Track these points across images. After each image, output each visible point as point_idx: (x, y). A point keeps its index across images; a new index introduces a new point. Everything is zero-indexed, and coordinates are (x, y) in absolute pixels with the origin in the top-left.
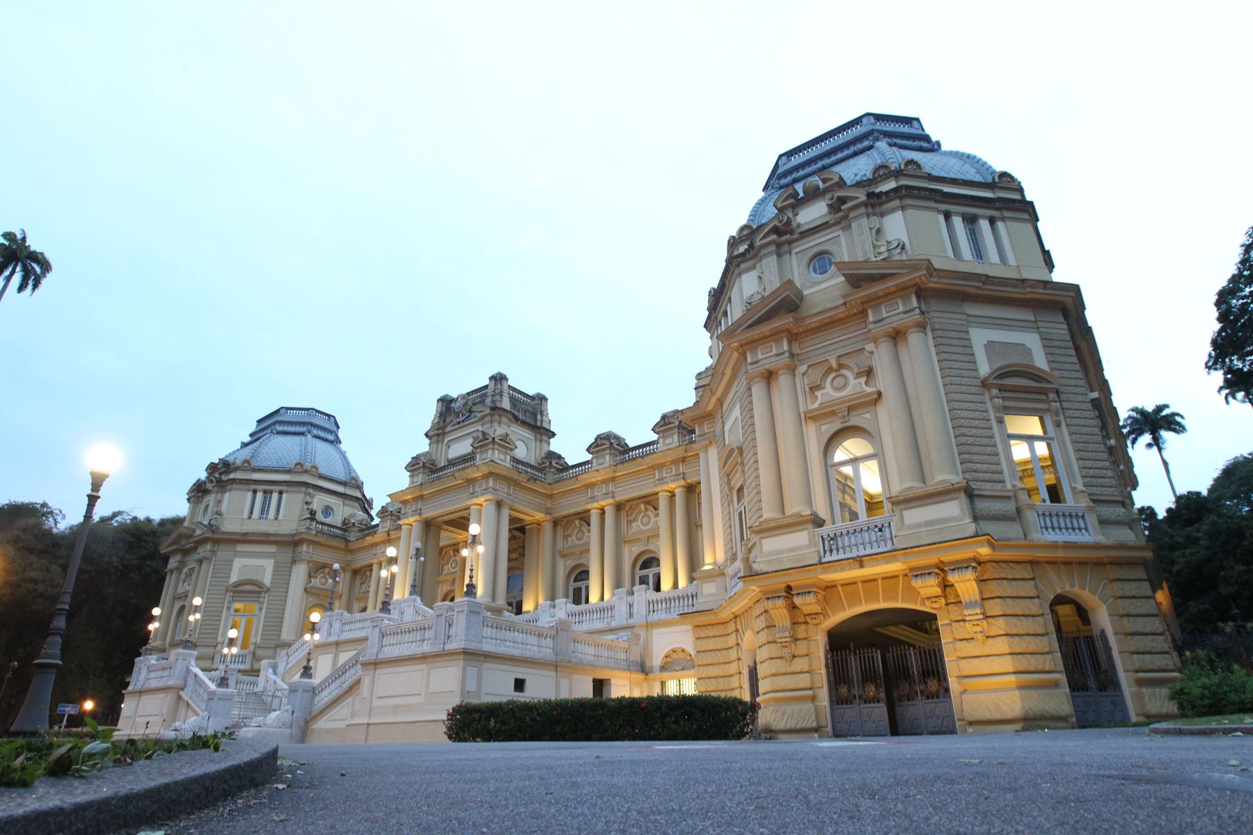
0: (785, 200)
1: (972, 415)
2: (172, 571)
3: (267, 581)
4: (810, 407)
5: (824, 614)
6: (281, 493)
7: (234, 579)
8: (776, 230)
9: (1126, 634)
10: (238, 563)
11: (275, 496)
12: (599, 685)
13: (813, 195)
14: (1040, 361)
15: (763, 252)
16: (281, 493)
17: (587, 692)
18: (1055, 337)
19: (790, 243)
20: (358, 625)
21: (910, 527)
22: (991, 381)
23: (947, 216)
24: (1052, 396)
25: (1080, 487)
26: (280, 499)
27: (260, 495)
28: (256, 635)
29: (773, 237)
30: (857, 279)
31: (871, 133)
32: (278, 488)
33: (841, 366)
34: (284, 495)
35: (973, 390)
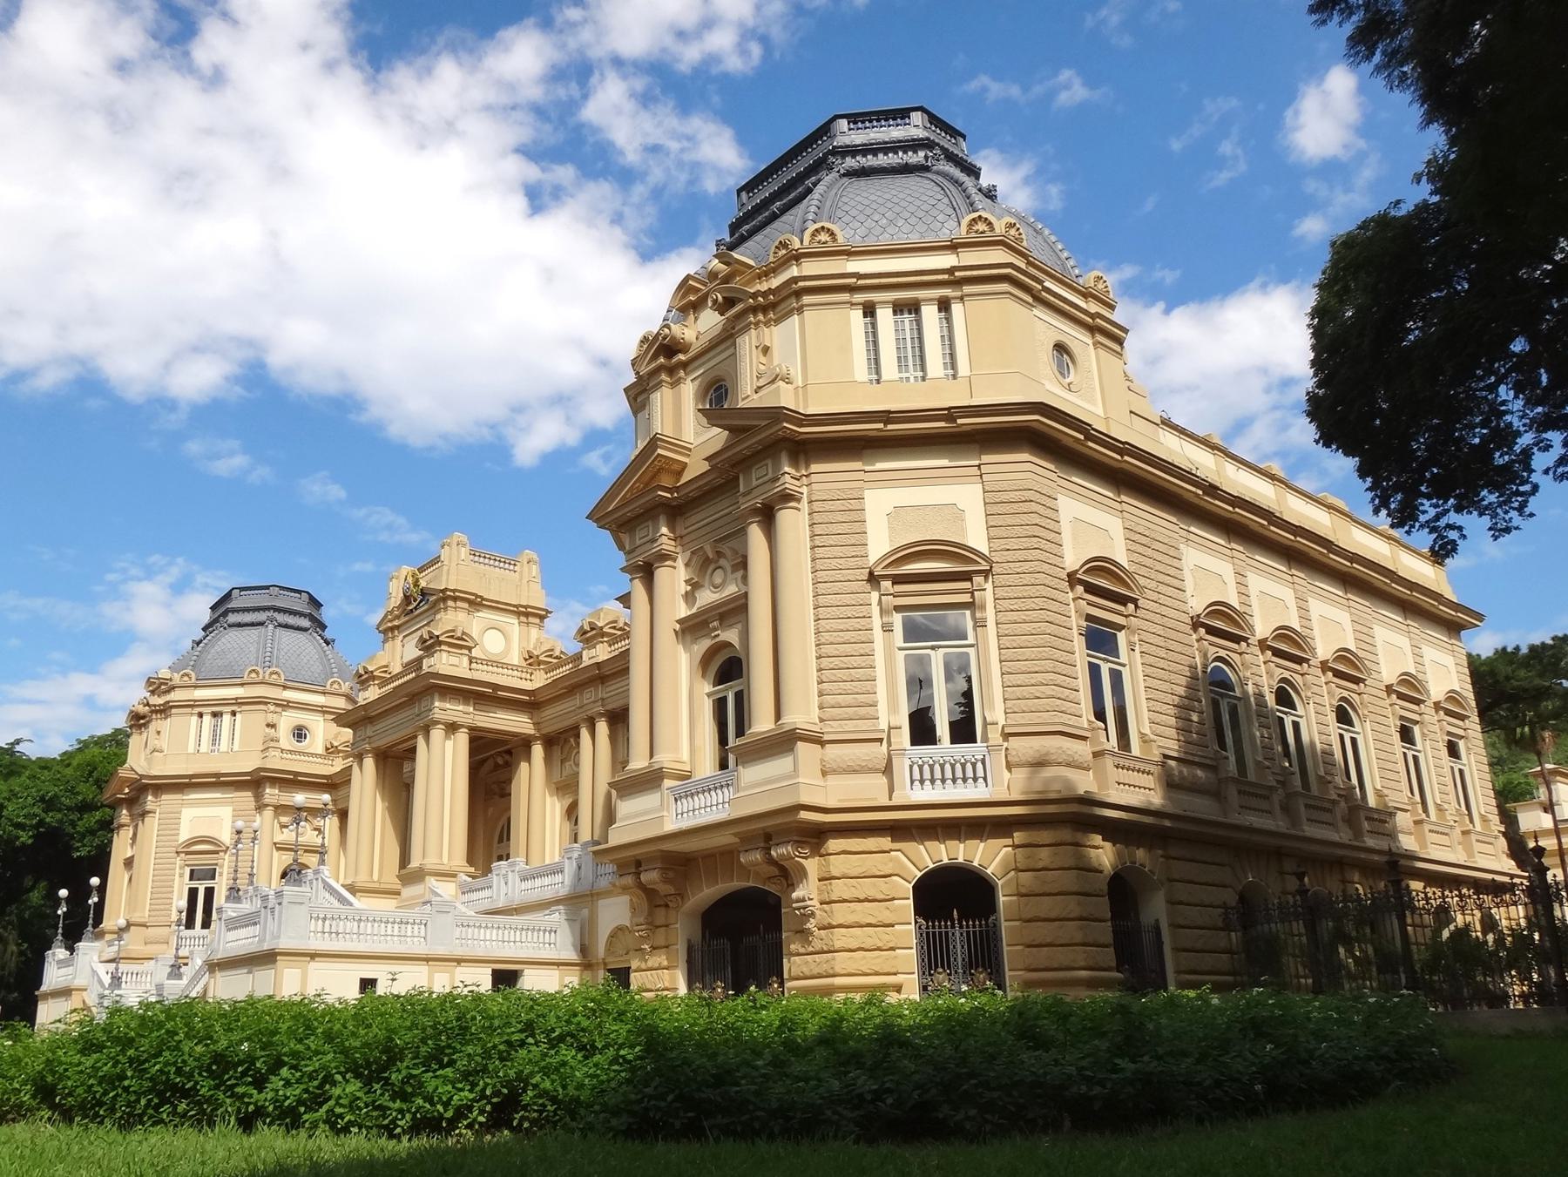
1: (842, 624)
3: (976, 537)
5: (681, 895)
7: (184, 836)
10: (188, 814)
12: (505, 978)
16: (234, 714)
17: (352, 993)
18: (1005, 486)
23: (869, 311)
31: (926, 144)
33: (719, 554)
34: (957, 309)
35: (855, 586)
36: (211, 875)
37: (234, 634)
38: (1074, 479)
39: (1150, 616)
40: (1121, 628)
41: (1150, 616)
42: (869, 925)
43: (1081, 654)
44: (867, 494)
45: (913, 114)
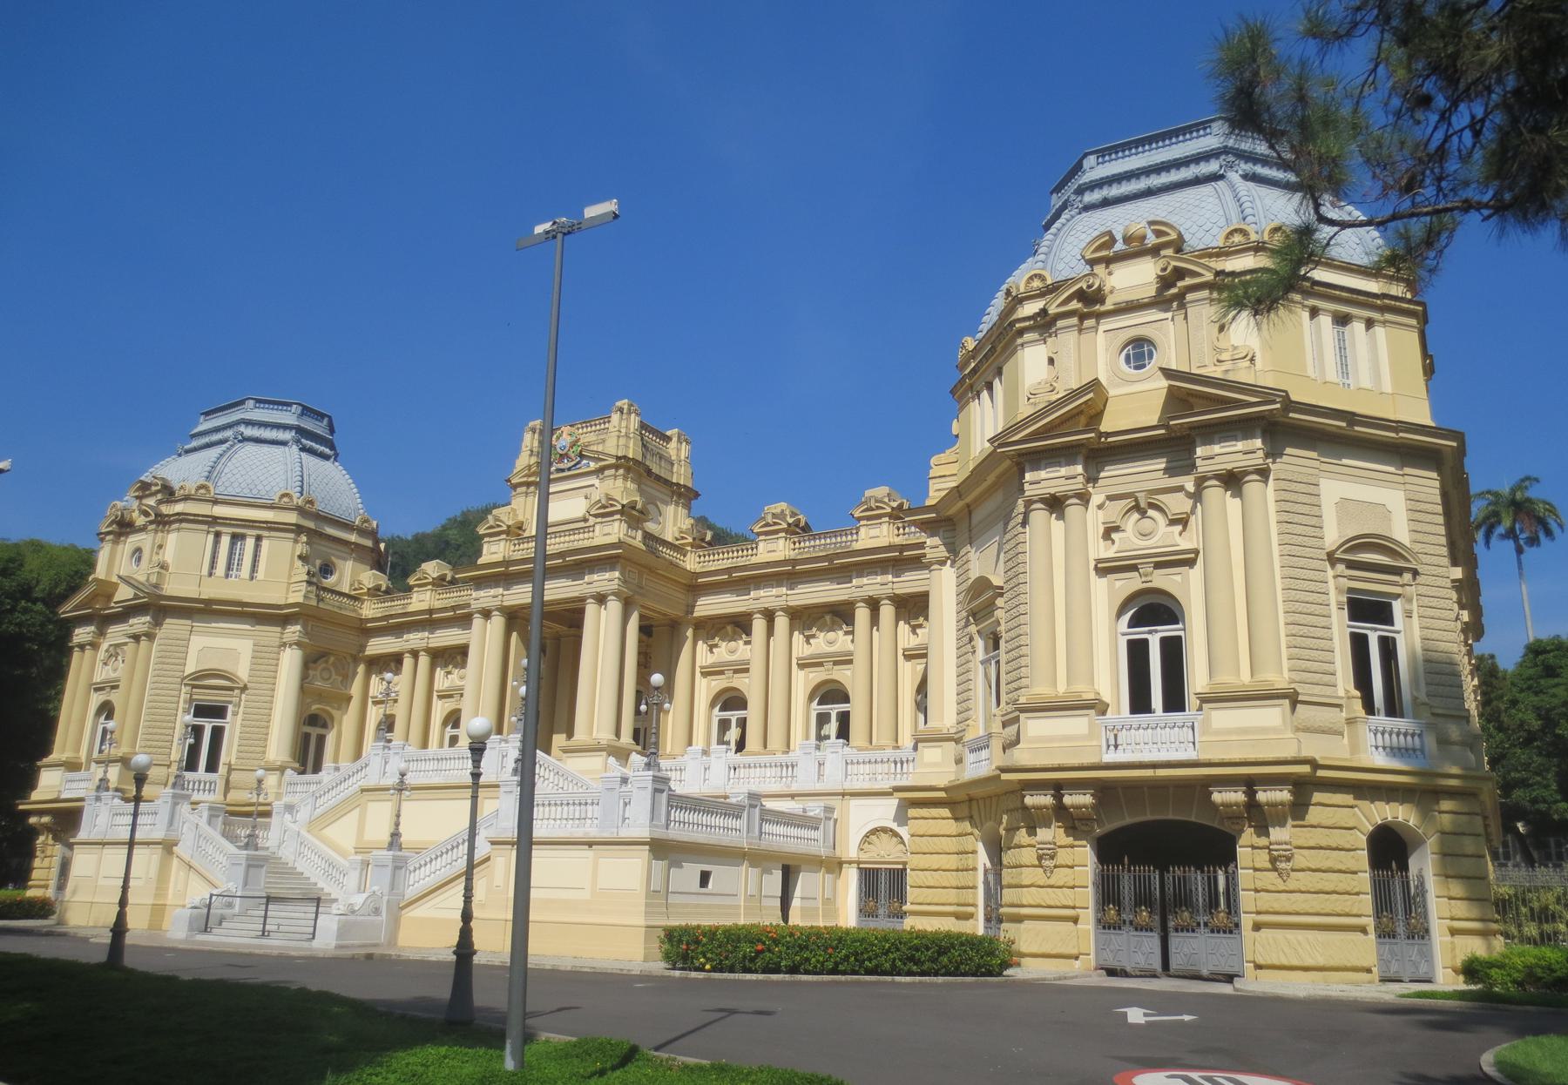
0: (1096, 250)
2: (82, 647)
3: (243, 672)
4: (1104, 555)
6: (259, 539)
7: (190, 668)
8: (1081, 295)
9: (1521, 574)
11: (250, 543)
13: (1137, 249)
14: (1401, 532)
15: (1060, 323)
16: (259, 539)
19: (1099, 316)
20: (431, 765)
21: (1218, 732)
22: (1338, 555)
24: (1407, 577)
25: (1423, 697)
26: (257, 547)
27: (225, 541)
28: (229, 754)
29: (1075, 305)
30: (1186, 394)
31: (1225, 151)
32: (255, 532)
34: (265, 543)
36: (218, 711)
37: (250, 448)
38: (1345, 461)
39: (1430, 580)
40: (1398, 596)
41: (1430, 580)
42: (1340, 871)
43: (1340, 627)
44: (1322, 482)
45: (1214, 125)
